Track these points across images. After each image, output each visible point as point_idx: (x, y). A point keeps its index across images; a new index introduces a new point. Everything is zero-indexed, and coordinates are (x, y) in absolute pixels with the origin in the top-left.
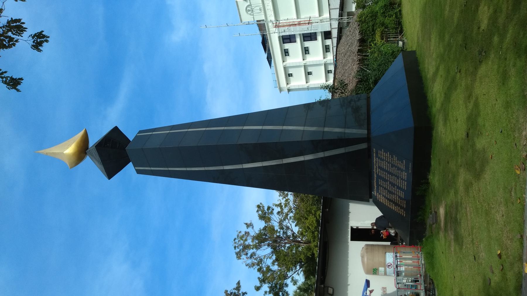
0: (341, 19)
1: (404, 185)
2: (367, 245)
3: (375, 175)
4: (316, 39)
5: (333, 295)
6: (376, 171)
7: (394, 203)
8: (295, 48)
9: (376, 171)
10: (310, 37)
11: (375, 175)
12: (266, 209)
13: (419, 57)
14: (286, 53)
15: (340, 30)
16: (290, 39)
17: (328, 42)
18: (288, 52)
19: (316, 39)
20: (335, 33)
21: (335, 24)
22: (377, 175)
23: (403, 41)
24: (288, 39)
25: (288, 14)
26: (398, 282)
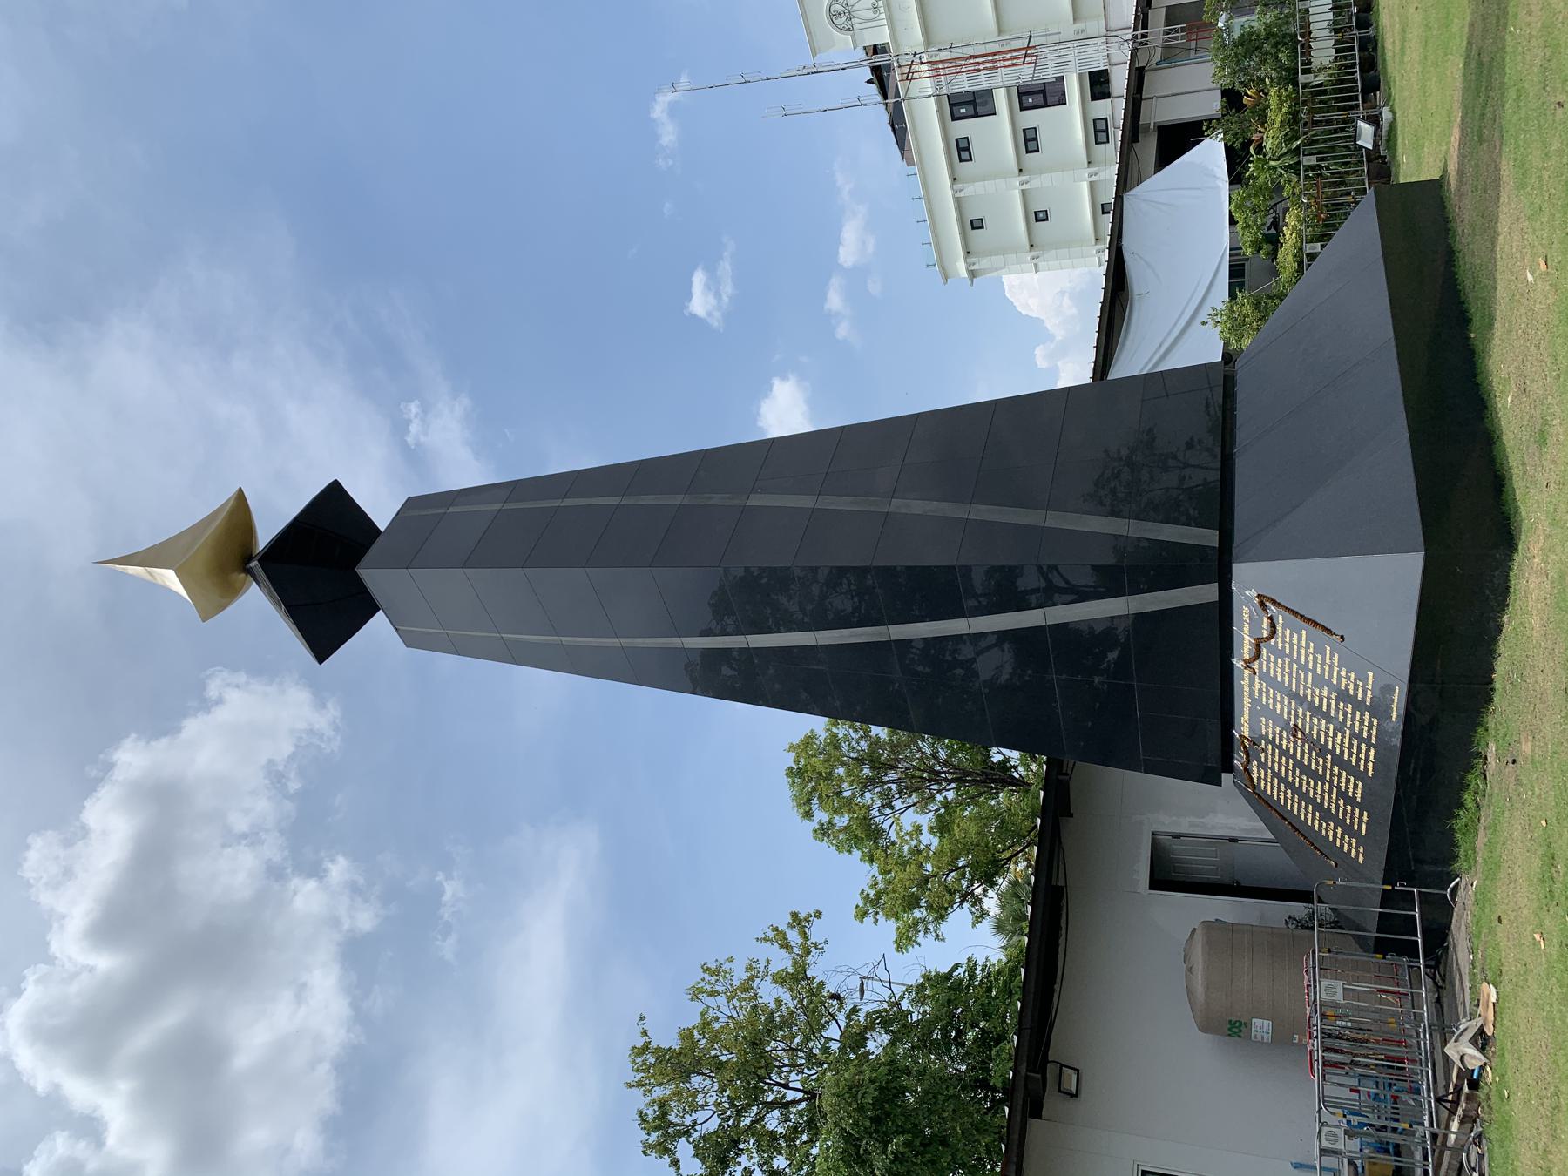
0: (1144, 36)
1: (1367, 760)
2: (1213, 928)
3: (1247, 700)
4: (1062, 102)
5: (1076, 1095)
6: (1251, 685)
7: (1318, 807)
8: (995, 134)
9: (1251, 685)
10: (1044, 95)
11: (1247, 700)
12: (773, 1006)
13: (1507, 629)
14: (963, 149)
15: (1138, 77)
16: (973, 103)
17: (1101, 108)
18: (968, 149)
19: (1062, 102)
20: (1120, 81)
21: (1123, 54)
22: (1256, 702)
23: (1375, 121)
24: (972, 105)
25: (972, 12)
26: (1326, 1144)
